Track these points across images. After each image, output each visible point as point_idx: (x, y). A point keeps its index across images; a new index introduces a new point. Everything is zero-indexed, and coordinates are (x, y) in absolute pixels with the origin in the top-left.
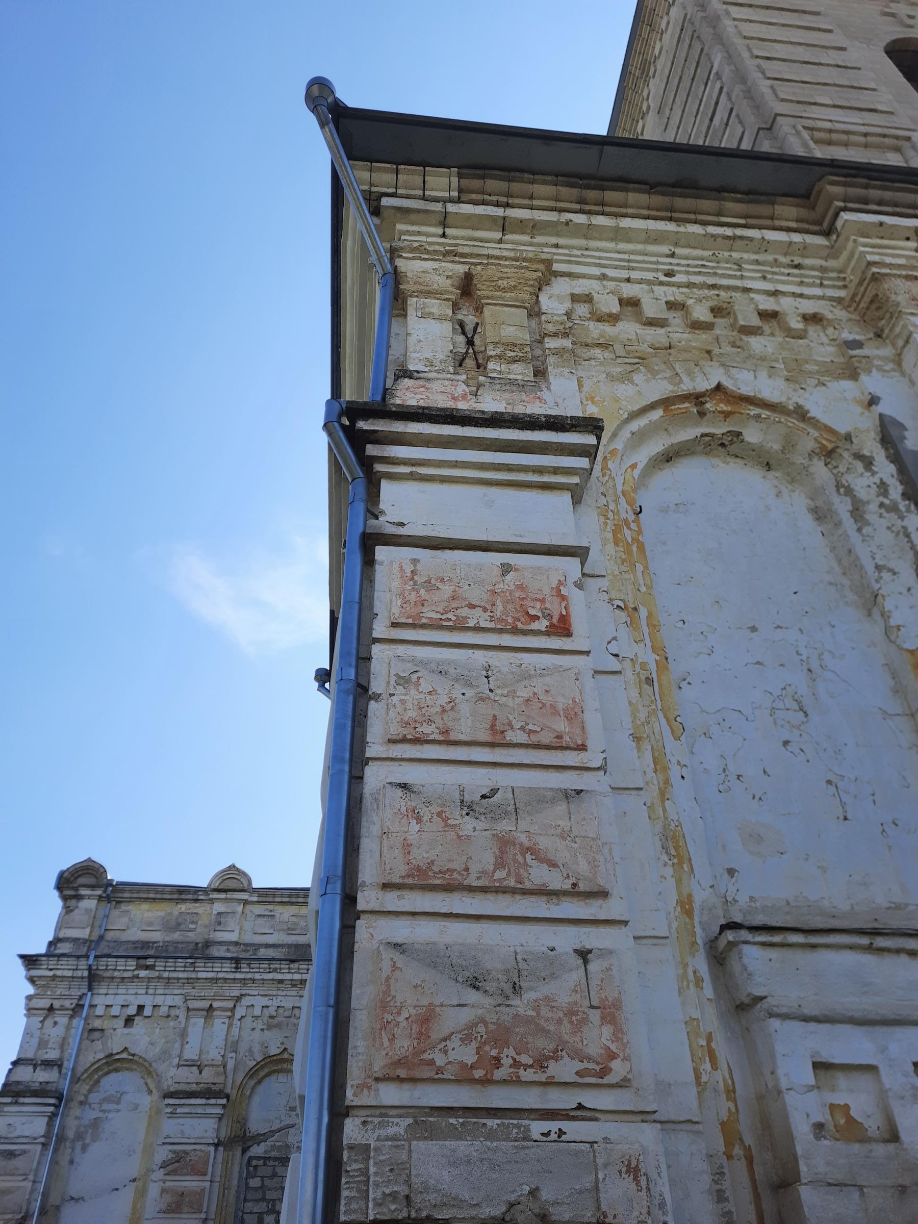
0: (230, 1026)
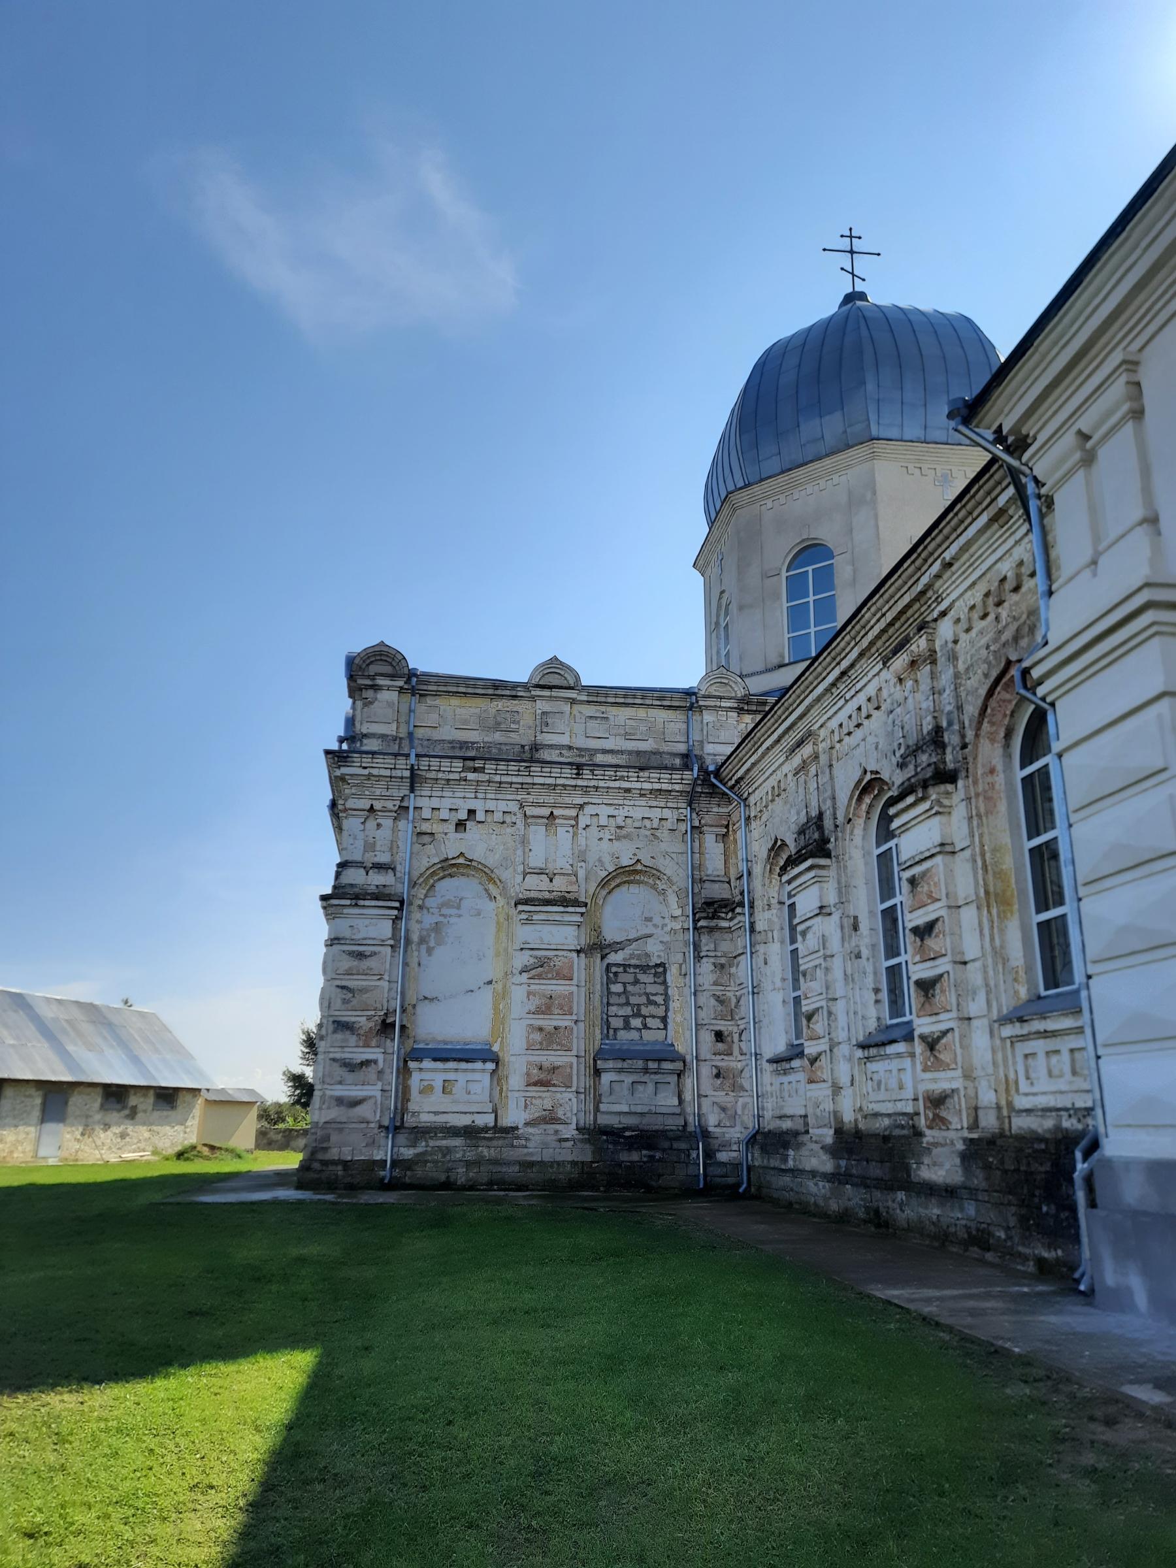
0: (575, 835)
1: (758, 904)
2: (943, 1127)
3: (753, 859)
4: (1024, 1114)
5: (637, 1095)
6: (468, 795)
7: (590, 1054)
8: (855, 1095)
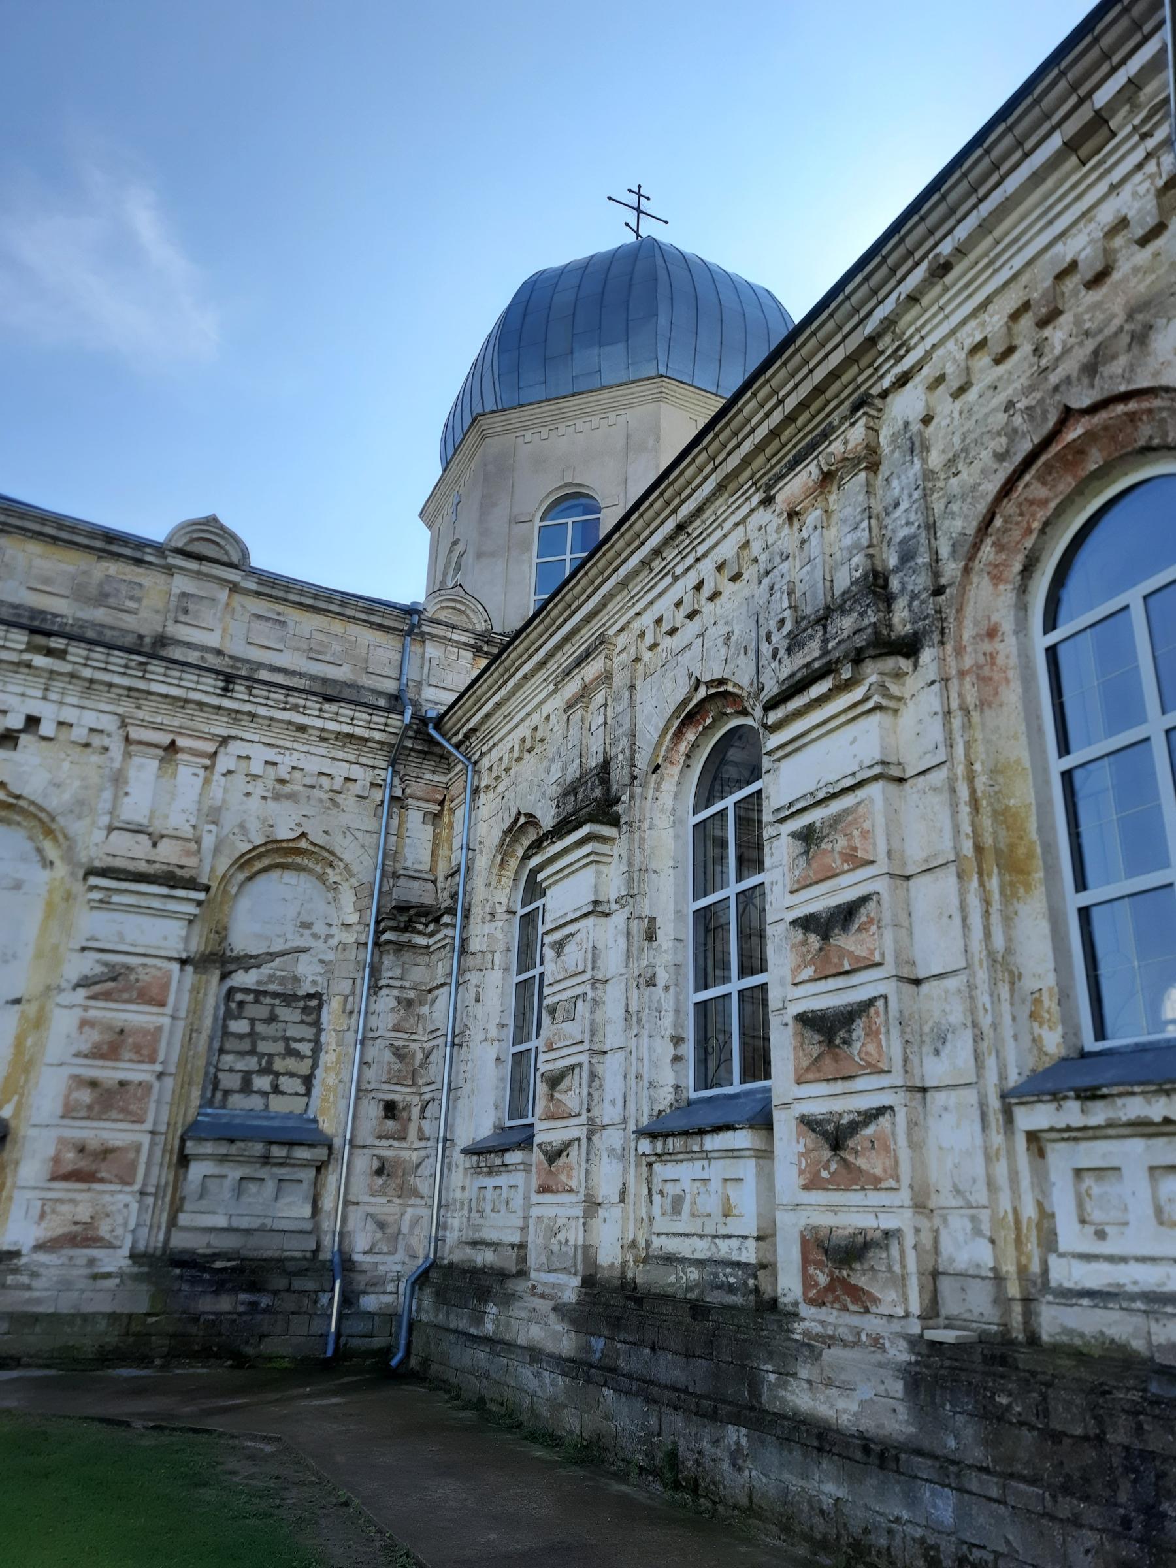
0: (207, 782)
1: (477, 912)
2: (852, 1307)
3: (477, 848)
4: (1085, 1302)
5: (245, 1199)
6: (30, 692)
7: (175, 1131)
8: (625, 1218)
